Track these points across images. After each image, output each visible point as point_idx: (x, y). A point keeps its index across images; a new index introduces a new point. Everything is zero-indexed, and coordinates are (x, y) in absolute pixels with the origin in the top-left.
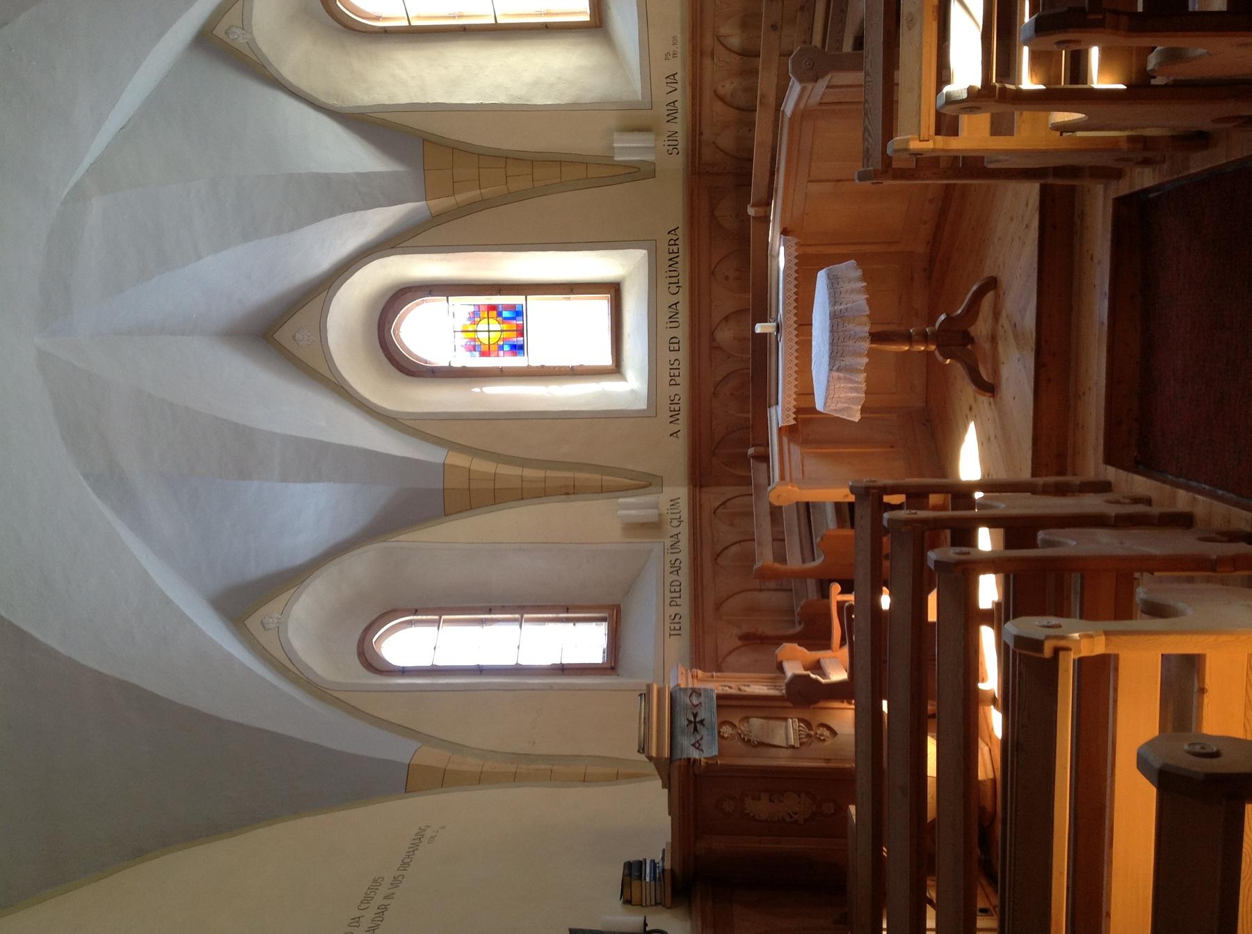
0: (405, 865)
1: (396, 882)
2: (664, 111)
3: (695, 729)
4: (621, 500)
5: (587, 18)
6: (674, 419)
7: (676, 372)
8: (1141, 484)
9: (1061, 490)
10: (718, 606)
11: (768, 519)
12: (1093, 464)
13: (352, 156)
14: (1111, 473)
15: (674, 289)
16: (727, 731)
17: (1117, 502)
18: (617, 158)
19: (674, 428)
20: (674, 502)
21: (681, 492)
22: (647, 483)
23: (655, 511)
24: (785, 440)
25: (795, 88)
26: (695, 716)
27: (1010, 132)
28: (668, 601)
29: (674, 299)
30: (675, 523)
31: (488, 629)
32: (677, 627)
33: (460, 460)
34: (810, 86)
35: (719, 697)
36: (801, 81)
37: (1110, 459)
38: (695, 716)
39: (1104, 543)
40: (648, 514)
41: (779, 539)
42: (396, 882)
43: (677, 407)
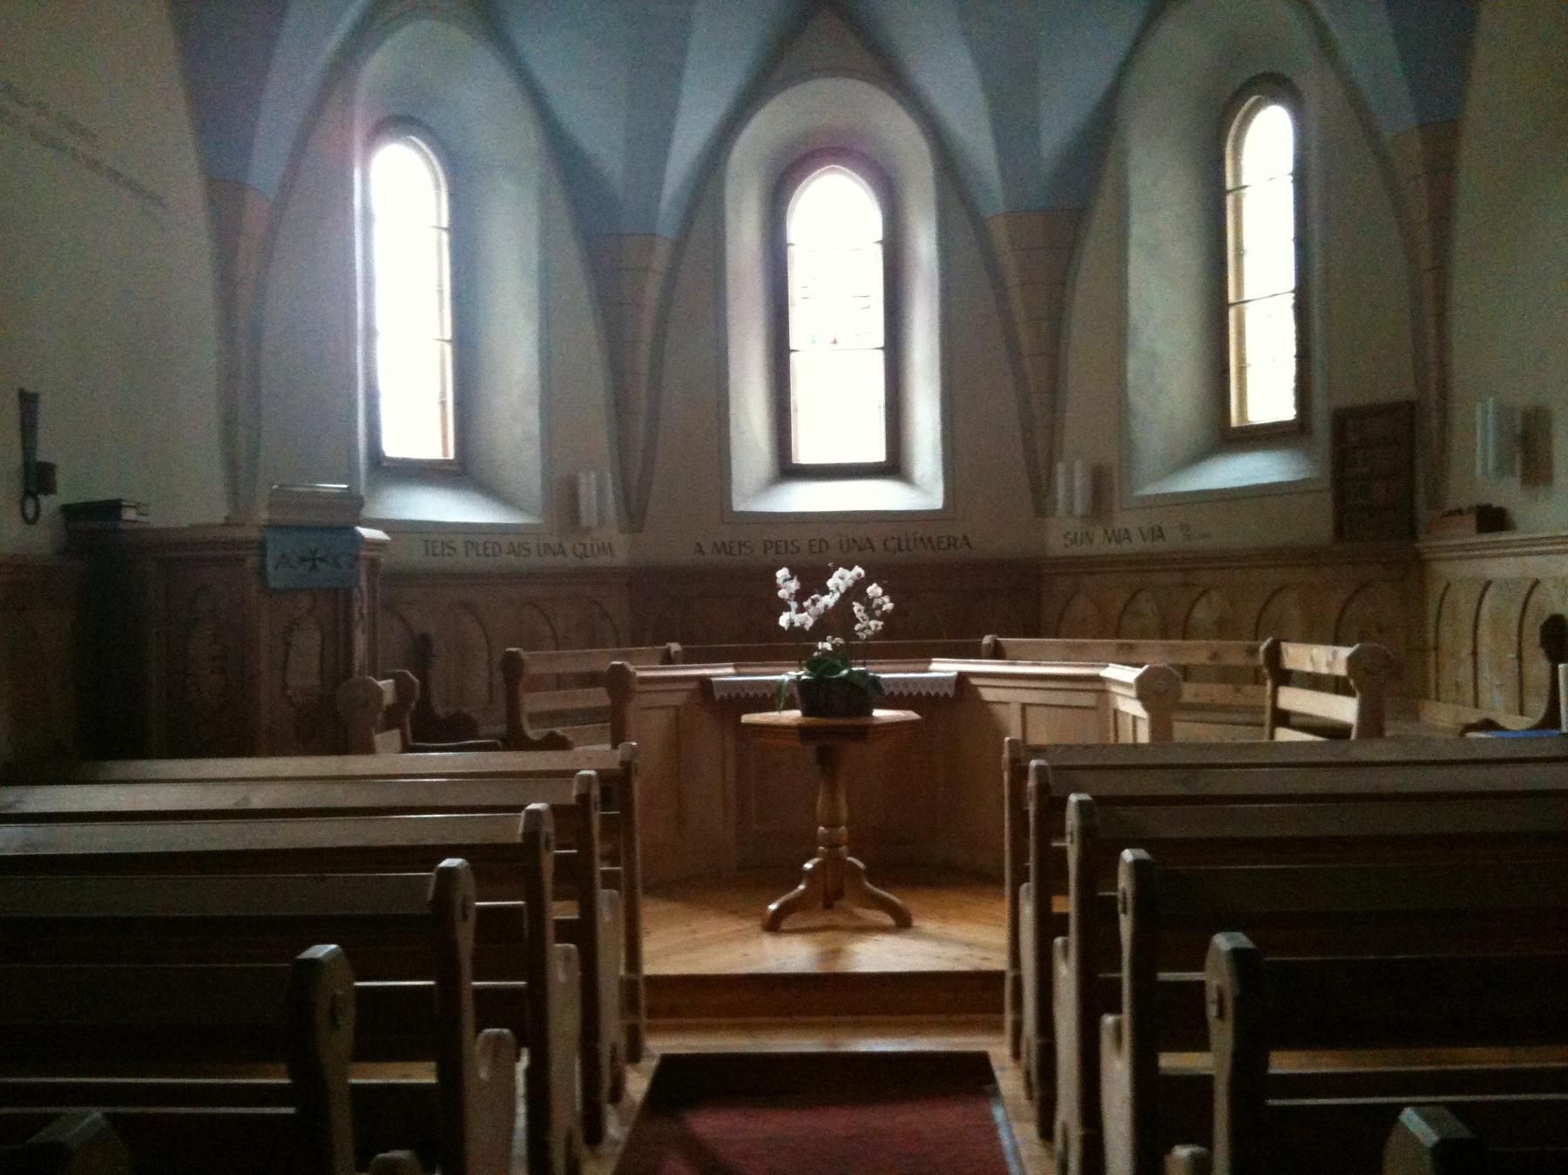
0: (115, 176)
1: (94, 164)
2: (1118, 525)
3: (303, 560)
4: (609, 475)
5: (1235, 421)
6: (723, 548)
7: (782, 549)
8: (637, 1084)
9: (630, 1002)
10: (467, 606)
11: (585, 669)
12: (659, 1045)
13: (1058, 123)
14: (650, 1065)
15: (892, 544)
16: (305, 602)
17: (613, 1059)
18: (1060, 468)
19: (707, 549)
20: (607, 548)
21: (621, 557)
22: (634, 513)
23: (594, 522)
24: (693, 685)
25: (1129, 674)
26: (322, 560)
27: (1066, 916)
28: (470, 538)
29: (878, 544)
30: (580, 549)
31: (380, 323)
32: (438, 550)
33: (660, 258)
34: (1133, 693)
35: (348, 591)
36: (1140, 680)
37: (669, 1063)
38: (322, 560)
39: (564, 1020)
40: (588, 514)
41: (560, 682)
42: (94, 164)
43: (735, 551)
